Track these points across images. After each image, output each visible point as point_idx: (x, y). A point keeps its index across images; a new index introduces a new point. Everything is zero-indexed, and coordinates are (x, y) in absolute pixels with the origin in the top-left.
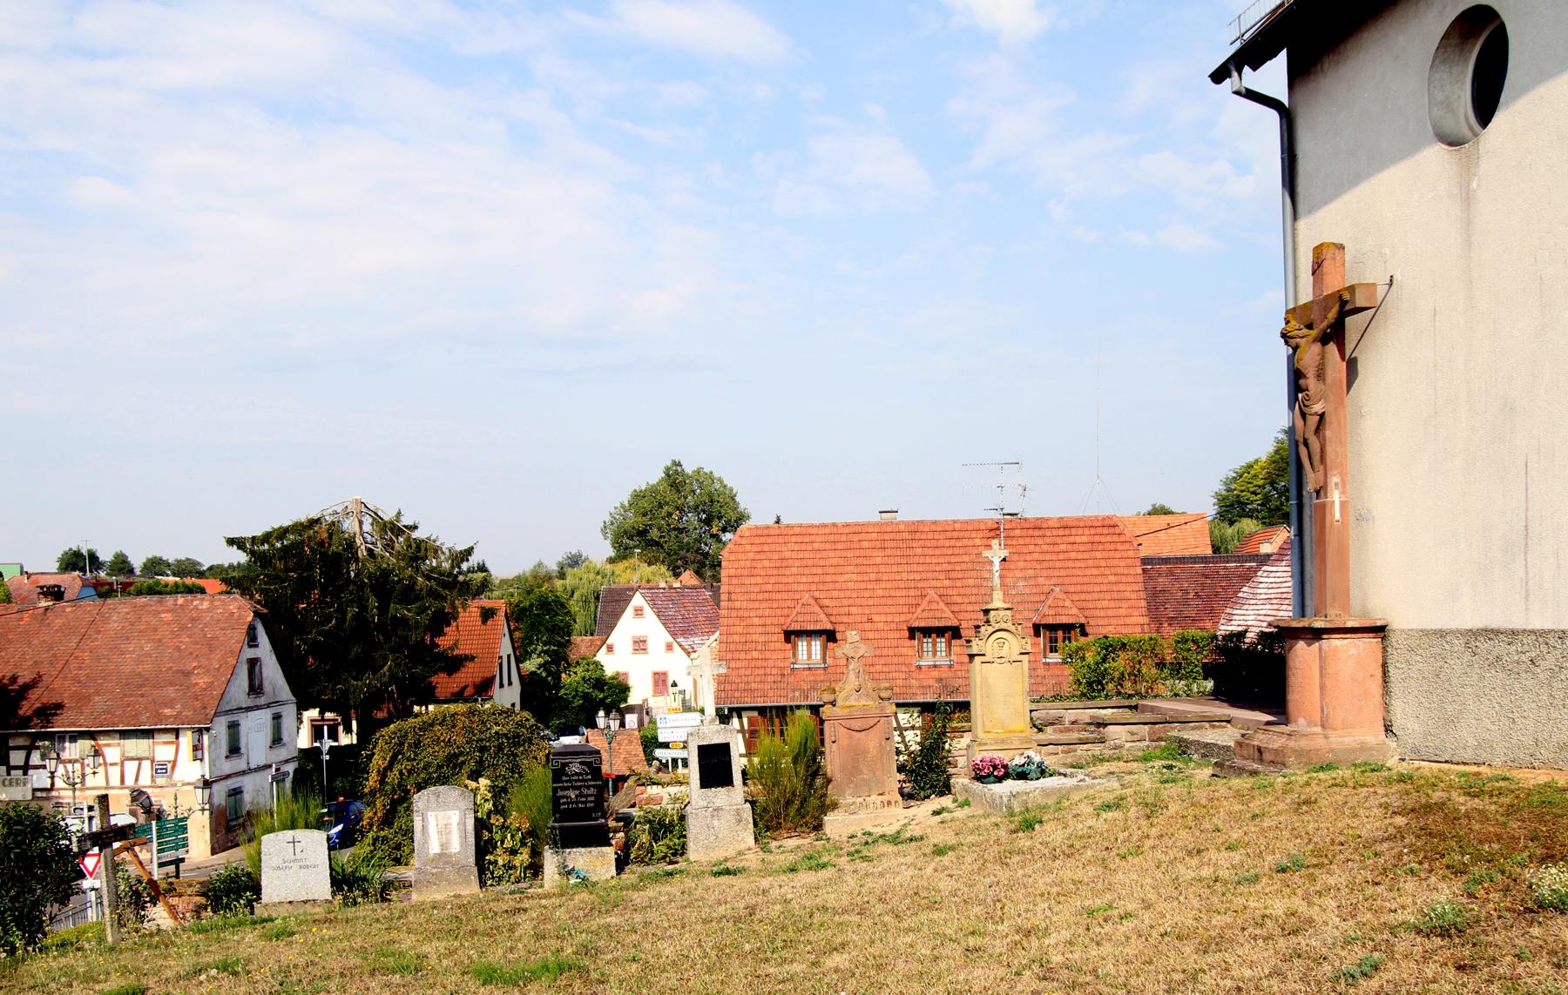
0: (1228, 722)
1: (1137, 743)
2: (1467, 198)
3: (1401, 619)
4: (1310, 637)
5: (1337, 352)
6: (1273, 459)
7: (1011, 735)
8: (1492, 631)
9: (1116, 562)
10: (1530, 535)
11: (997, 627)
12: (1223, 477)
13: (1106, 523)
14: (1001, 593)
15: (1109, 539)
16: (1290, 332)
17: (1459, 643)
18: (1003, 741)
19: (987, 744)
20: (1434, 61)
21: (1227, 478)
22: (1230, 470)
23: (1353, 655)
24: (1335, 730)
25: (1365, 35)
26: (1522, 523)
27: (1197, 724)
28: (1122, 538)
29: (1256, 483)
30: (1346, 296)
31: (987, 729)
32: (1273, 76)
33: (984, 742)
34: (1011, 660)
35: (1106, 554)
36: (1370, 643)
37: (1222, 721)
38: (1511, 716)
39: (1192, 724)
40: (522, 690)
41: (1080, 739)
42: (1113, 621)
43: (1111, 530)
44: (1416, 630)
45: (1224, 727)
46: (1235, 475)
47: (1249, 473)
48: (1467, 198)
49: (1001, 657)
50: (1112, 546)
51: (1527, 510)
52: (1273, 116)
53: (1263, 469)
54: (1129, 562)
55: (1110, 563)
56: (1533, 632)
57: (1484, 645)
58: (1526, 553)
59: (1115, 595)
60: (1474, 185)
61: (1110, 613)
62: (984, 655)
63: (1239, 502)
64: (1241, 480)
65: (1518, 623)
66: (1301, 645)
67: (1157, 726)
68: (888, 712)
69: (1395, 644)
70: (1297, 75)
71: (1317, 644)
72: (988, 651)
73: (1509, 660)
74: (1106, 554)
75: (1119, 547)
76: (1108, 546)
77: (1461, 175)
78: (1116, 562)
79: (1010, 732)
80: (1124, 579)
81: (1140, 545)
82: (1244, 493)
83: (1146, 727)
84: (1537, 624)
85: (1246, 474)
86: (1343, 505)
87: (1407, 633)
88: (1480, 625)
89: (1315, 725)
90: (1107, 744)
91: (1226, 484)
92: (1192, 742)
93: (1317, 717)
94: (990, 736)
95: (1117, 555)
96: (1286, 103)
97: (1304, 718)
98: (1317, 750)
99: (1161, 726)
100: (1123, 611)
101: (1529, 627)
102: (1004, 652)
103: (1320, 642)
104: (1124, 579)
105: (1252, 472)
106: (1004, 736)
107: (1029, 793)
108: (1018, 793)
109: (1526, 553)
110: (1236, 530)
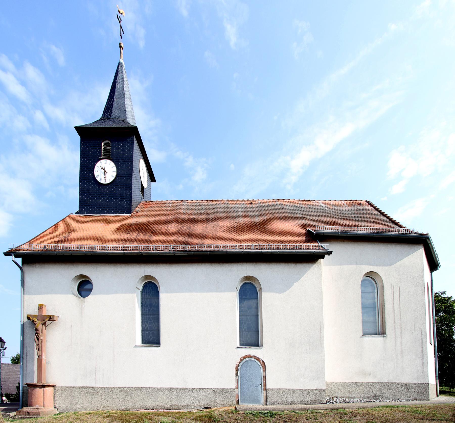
2: (82, 308)
3: (57, 385)
4: (41, 387)
8: (87, 387)
17: (77, 389)
20: (72, 280)
26: (95, 368)
30: (52, 317)
36: (51, 389)
48: (82, 308)
51: (96, 366)
58: (96, 373)
60: (84, 306)
66: (38, 389)
71: (42, 389)
77: (80, 303)
84: (98, 386)
86: (45, 360)
88: (83, 386)
89: (42, 406)
93: (42, 404)
96: (21, 267)
97: (38, 405)
98: (45, 411)
109: (96, 373)
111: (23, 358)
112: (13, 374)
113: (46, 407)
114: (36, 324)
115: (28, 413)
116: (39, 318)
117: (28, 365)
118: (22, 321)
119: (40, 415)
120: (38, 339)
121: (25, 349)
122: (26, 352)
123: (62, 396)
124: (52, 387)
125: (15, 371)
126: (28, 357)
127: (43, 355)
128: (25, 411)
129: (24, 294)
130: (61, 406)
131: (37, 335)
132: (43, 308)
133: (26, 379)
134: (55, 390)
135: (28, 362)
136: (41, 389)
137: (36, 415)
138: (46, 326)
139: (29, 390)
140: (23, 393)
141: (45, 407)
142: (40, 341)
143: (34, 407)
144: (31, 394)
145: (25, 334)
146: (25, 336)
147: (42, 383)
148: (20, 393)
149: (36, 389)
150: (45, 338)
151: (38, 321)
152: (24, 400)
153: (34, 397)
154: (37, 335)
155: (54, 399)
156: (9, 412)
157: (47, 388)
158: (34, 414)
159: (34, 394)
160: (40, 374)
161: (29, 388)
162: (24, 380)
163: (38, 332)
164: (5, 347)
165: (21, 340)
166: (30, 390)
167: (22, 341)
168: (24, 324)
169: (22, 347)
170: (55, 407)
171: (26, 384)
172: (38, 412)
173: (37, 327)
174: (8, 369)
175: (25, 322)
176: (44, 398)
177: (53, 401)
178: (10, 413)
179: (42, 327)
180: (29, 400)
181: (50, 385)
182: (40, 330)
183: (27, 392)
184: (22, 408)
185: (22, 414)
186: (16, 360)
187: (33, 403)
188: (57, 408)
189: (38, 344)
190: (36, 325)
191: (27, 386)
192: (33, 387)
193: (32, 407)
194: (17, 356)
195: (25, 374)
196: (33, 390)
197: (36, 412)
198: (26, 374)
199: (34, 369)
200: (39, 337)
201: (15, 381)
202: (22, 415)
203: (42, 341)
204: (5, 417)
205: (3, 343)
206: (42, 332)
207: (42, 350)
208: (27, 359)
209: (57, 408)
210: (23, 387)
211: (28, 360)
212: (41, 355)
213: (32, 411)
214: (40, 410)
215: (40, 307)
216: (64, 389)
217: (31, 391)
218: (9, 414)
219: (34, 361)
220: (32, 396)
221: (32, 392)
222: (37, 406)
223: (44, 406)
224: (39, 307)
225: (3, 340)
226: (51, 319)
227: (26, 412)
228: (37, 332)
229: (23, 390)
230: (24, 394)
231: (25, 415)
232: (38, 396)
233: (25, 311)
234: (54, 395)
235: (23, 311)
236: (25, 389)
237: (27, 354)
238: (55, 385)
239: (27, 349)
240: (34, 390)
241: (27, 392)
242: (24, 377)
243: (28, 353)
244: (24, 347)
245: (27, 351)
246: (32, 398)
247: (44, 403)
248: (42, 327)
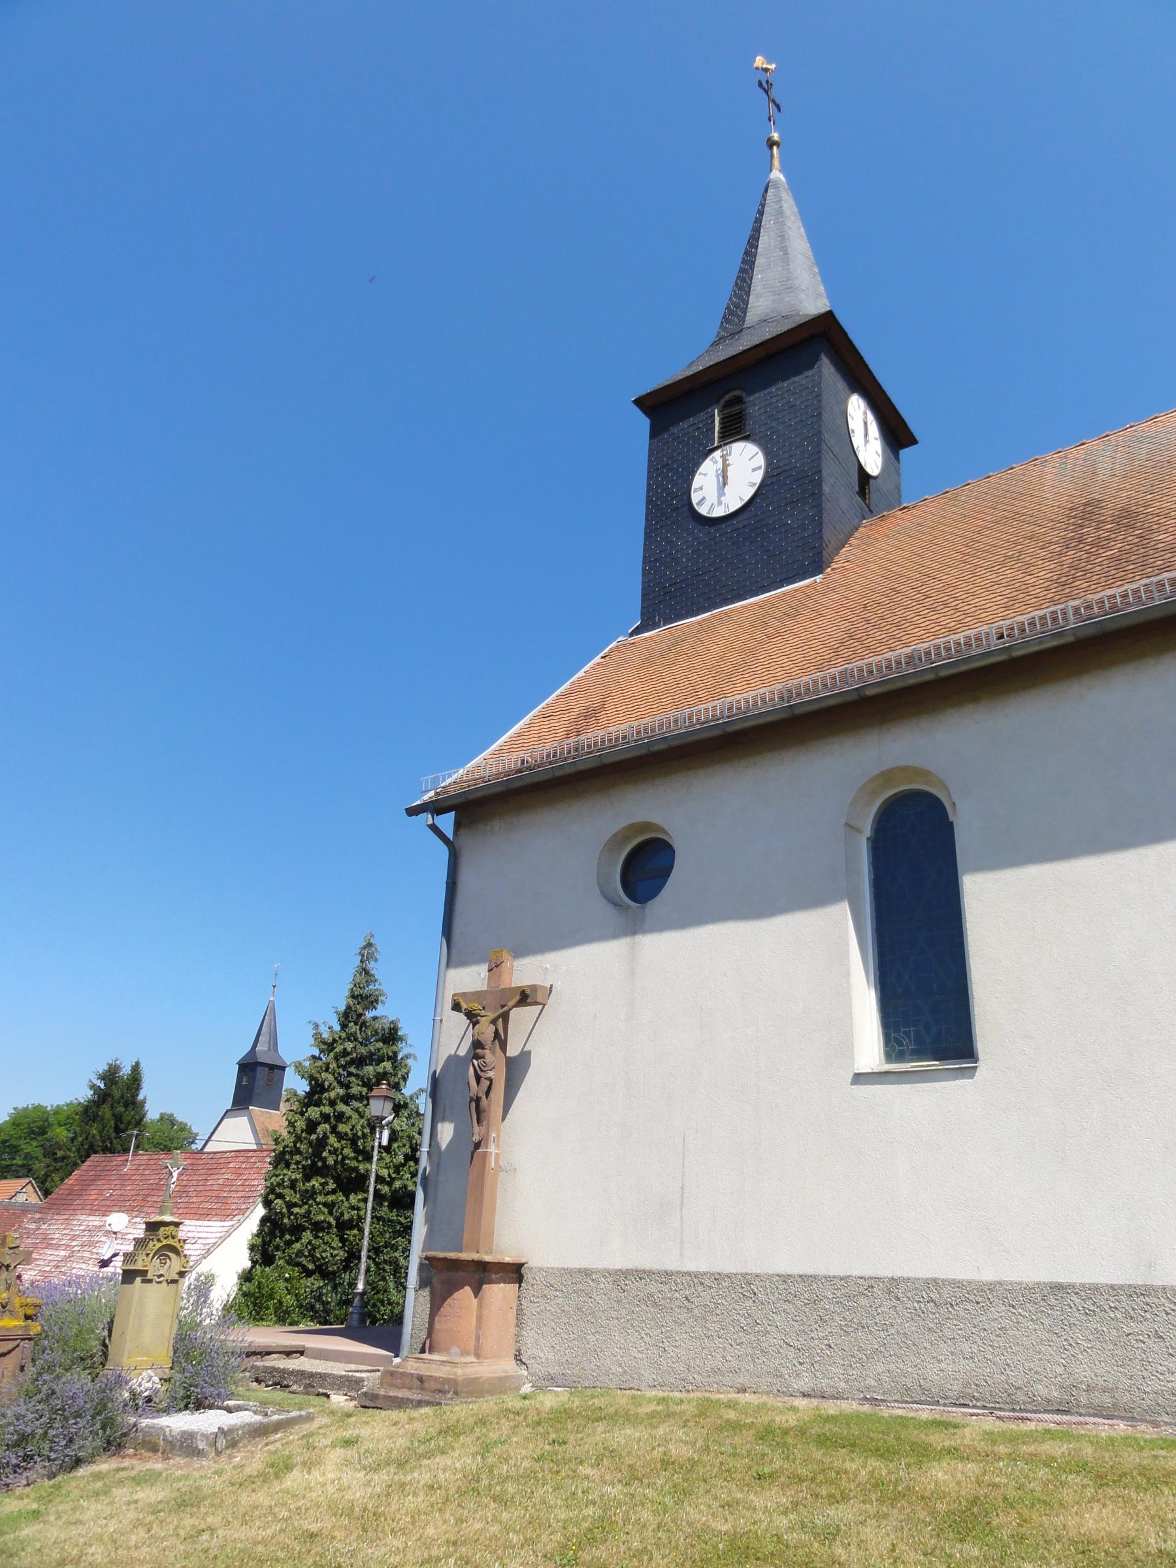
8: (644, 1271)
10: (685, 1195)
17: (605, 1284)
24: (487, 1359)
25: (497, 824)
32: (446, 822)
38: (661, 1345)
40: (453, 1138)
44: (557, 1269)
52: (444, 851)
56: (688, 1273)
57: (633, 1285)
65: (671, 1265)
68: (32, 1333)
69: (531, 1280)
70: (458, 825)
73: (661, 1296)
86: (497, 1155)
87: (549, 1271)
97: (459, 1347)
101: (685, 1269)
115: (421, 1379)
158: (438, 1386)
191: (427, 1262)
238: (523, 1261)
247: (478, 1338)
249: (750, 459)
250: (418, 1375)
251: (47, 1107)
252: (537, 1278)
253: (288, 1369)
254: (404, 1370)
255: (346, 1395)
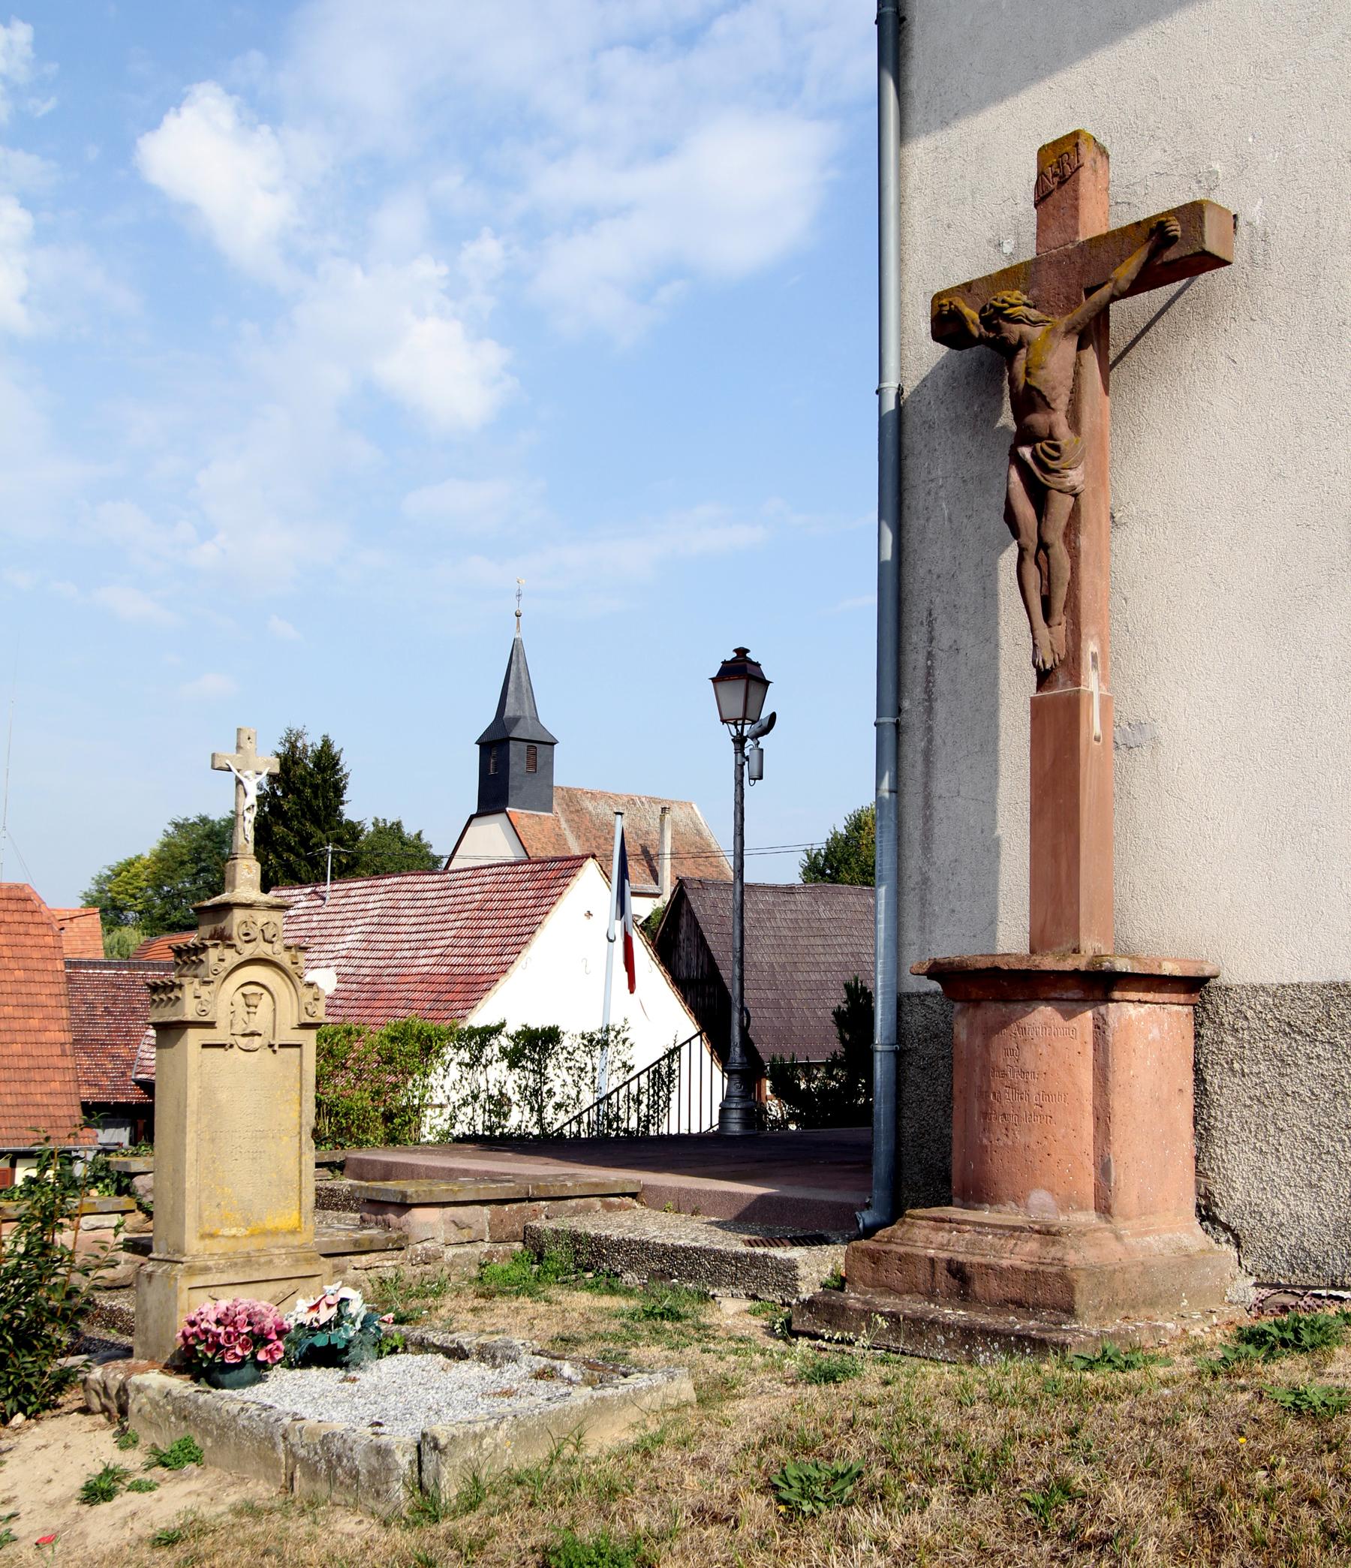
0: (633, 1195)
1: (468, 1248)
5: (1096, 361)
6: (163, 855)
7: (269, 1241)
9: (27, 952)
11: (249, 951)
12: (95, 874)
13: (12, 894)
14: (256, 867)
15: (17, 917)
16: (1012, 306)
18: (249, 1261)
19: (206, 1270)
21: (100, 876)
22: (105, 867)
23: (1154, 1040)
27: (582, 1201)
28: (37, 918)
29: (136, 884)
30: (1175, 228)
31: (207, 1229)
33: (199, 1263)
34: (277, 1042)
35: (12, 940)
37: (624, 1195)
39: (573, 1203)
41: (356, 1242)
42: (20, 1037)
43: (21, 905)
45: (630, 1207)
46: (109, 873)
47: (128, 871)
49: (253, 1034)
50: (22, 929)
53: (146, 868)
54: (47, 952)
55: (18, 952)
59: (24, 1000)
61: (16, 1025)
62: (210, 1025)
63: (115, 908)
64: (119, 879)
66: (1043, 1016)
67: (507, 1208)
71: (1089, 1014)
72: (220, 1013)
74: (12, 940)
75: (32, 930)
76: (15, 928)
78: (27, 952)
79: (266, 1233)
80: (37, 977)
81: (63, 929)
82: (121, 896)
83: (486, 1210)
85: (124, 873)
86: (1105, 701)
89: (1082, 1208)
90: (408, 1253)
91: (98, 883)
92: (618, 1246)
93: (1087, 1185)
94: (216, 1246)
95: (29, 941)
97: (1051, 1190)
98: (1123, 1270)
99: (515, 1206)
100: (34, 1023)
102: (260, 1019)
103: (1102, 1009)
104: (37, 977)
105: (133, 870)
106: (251, 1246)
107: (482, 1437)
108: (453, 1438)
110: (116, 940)
111: (897, 725)
112: (812, 941)
113: (1127, 1218)
114: (1021, 344)
115: (958, 1272)
116: (1050, 279)
117: (941, 785)
118: (891, 385)
119: (1080, 1308)
120: (1039, 496)
121: (916, 637)
122: (921, 673)
123: (1290, 1089)
124: (1182, 998)
125: (824, 925)
126: (939, 706)
127: (1087, 660)
128: (931, 1252)
129: (903, 137)
130: (1280, 1206)
131: (1026, 452)
132: (1085, 174)
133: (922, 929)
134: (1207, 1032)
135: (940, 763)
136: (1074, 1023)
137: (1038, 1306)
138: (1112, 356)
139: (961, 1031)
140: (900, 1057)
141: (1119, 1222)
142: (1061, 506)
143: (1007, 1215)
144: (977, 1079)
145: (917, 499)
146: (912, 536)
147: (1076, 951)
148: (878, 1057)
149: (1027, 1013)
150: (1099, 475)
151: (1034, 314)
152: (910, 1128)
153: (1007, 1101)
154: (1034, 456)
155: (1203, 1130)
156: (796, 1242)
157: (1132, 1011)
158: (1014, 1292)
159: (1004, 1075)
160: (1055, 855)
161: (958, 1006)
162: (911, 935)
163: (1038, 419)
164: (765, 714)
165: (881, 565)
166: (970, 1026)
167: (890, 573)
168: (908, 410)
169: (890, 645)
170: (1214, 1220)
171: (937, 971)
172: (1061, 1276)
173: (1028, 373)
174: (789, 916)
175: (916, 392)
176: (1103, 1118)
177: (1187, 1144)
178: (796, 1253)
179: (1078, 364)
180: (956, 1132)
181: (1169, 969)
182: (1061, 403)
183: (931, 1050)
184: (895, 1214)
185: (895, 1277)
186: (828, 871)
187: (1000, 1165)
188: (1234, 1224)
189: (1043, 546)
190: (1023, 351)
191: (935, 986)
192: (995, 1000)
193: (985, 1215)
194: (829, 849)
195: (912, 880)
196: (992, 1030)
197: (1035, 1277)
198: (925, 880)
199: (994, 820)
200: (1052, 464)
201: (822, 986)
202: (898, 1293)
203: (1075, 514)
204: (759, 1288)
205: (754, 688)
206: (1075, 423)
207: (1073, 606)
208: (930, 729)
209: (1227, 1228)
210: (902, 1002)
211: (938, 741)
212: (1072, 662)
213: (990, 1260)
214: (1072, 1258)
215: (1049, 172)
216: (1316, 1013)
217: (978, 1041)
218: (791, 1266)
219: (996, 739)
220: (984, 1094)
221: (987, 1047)
222: (1041, 1204)
223: (1104, 1209)
224: (1041, 174)
225: (758, 665)
226: (1171, 254)
227: (932, 1261)
228: (1030, 427)
229: (900, 1032)
230: (911, 1072)
231: (931, 1296)
232: (1047, 1095)
233: (910, 287)
234: (1200, 1080)
235: (901, 290)
236: (916, 1019)
237: (928, 692)
238: (1207, 971)
239: (931, 640)
240: (1005, 1024)
241: (931, 1050)
242: (911, 902)
243: (940, 675)
244: (906, 620)
245: (930, 655)
246: (985, 1115)
247: (1104, 1169)
248: (1078, 364)
249: (204, 1046)
250: (950, 1262)
251: (839, 1007)
252: (1250, 1014)
253: (607, 1238)
254: (908, 1249)
255: (754, 1297)
